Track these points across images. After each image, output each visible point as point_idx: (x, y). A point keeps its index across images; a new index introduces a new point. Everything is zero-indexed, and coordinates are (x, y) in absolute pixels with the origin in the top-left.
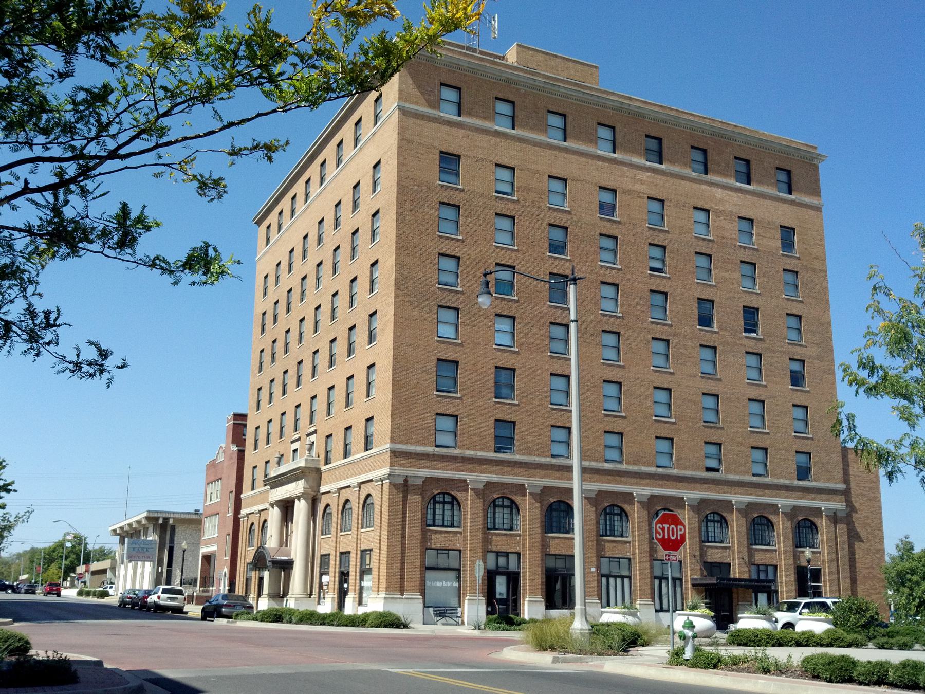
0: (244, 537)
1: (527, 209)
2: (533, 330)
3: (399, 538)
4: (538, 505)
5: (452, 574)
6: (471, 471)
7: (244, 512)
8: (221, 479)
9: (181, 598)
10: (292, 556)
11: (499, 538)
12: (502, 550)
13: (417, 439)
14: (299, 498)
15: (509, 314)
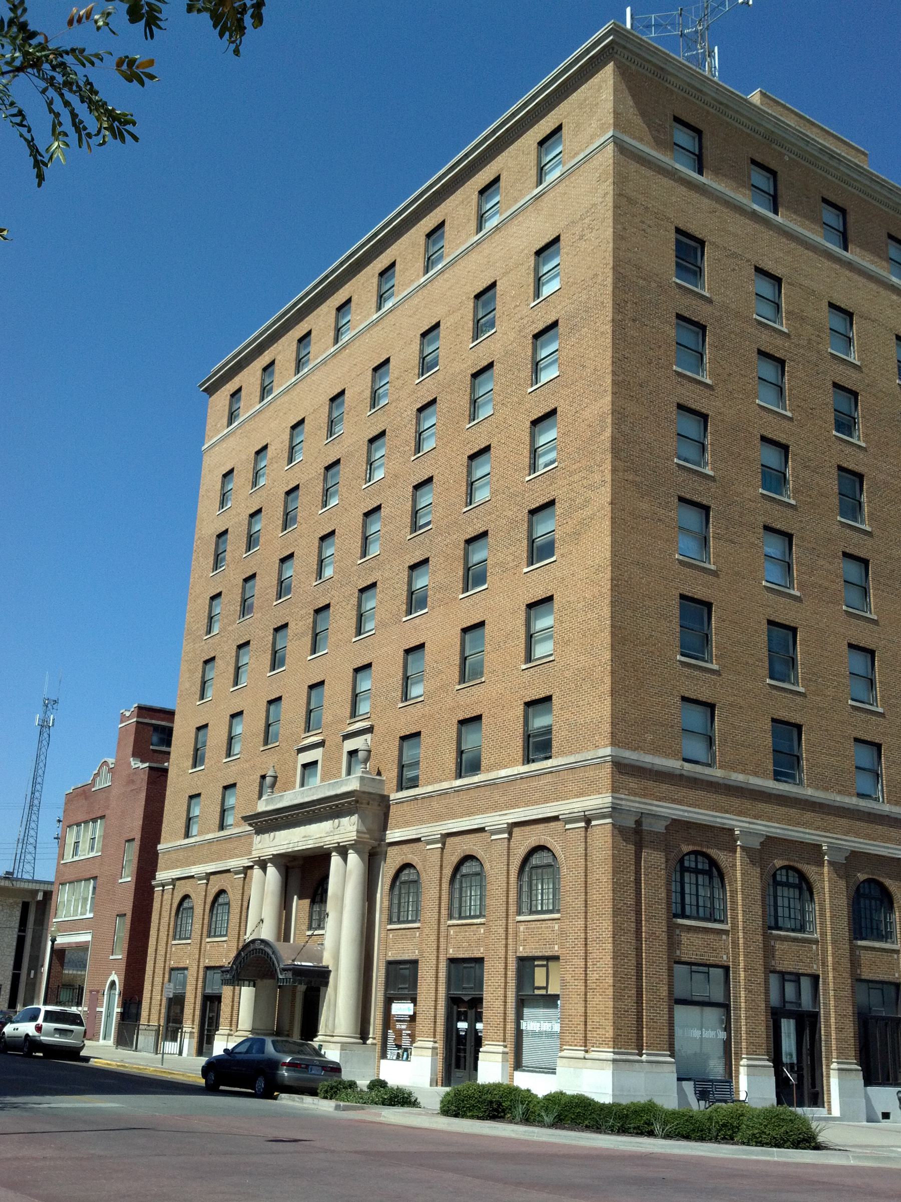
0: (165, 920)
1: (802, 351)
2: (821, 562)
3: (631, 937)
4: (842, 884)
5: (713, 1015)
6: (740, 813)
7: (162, 875)
8: (102, 817)
9: (79, 1032)
10: (327, 960)
11: (785, 945)
12: (791, 969)
13: (653, 743)
14: (343, 851)
15: (783, 528)
